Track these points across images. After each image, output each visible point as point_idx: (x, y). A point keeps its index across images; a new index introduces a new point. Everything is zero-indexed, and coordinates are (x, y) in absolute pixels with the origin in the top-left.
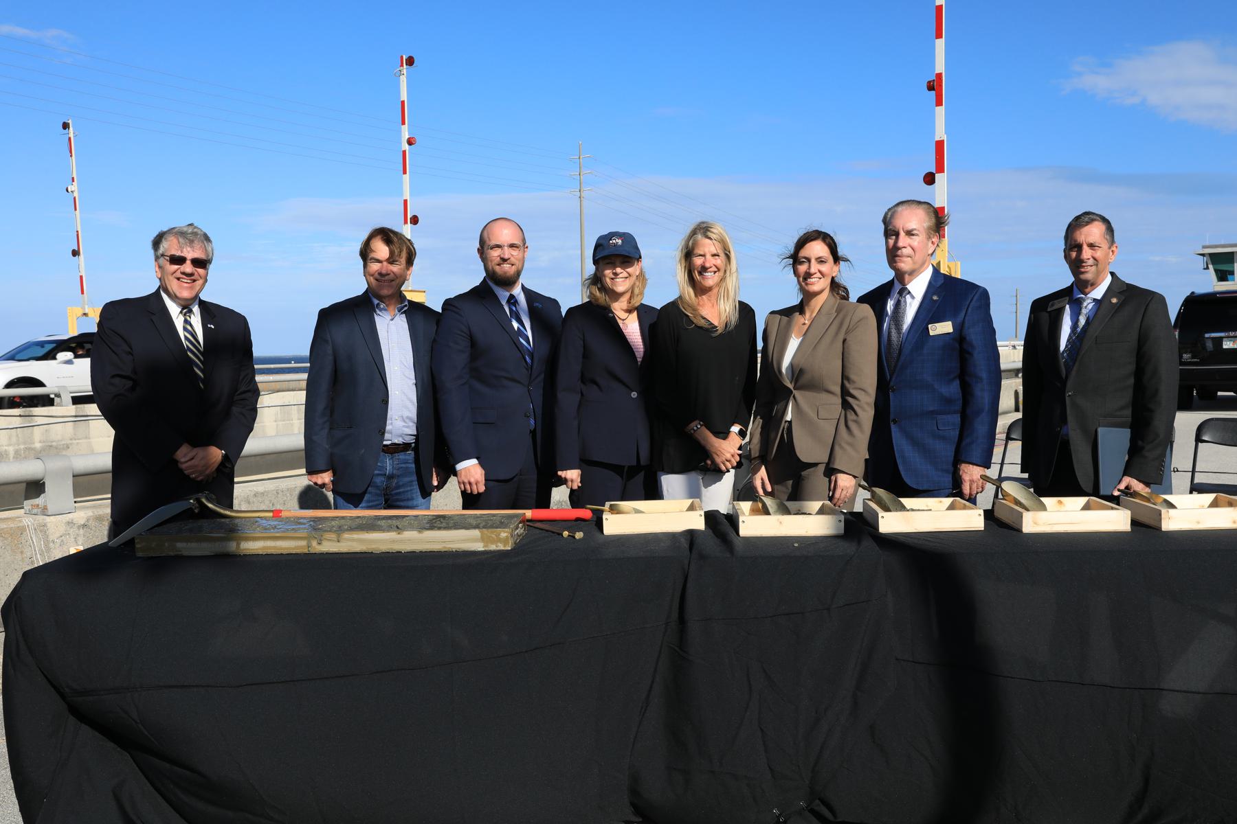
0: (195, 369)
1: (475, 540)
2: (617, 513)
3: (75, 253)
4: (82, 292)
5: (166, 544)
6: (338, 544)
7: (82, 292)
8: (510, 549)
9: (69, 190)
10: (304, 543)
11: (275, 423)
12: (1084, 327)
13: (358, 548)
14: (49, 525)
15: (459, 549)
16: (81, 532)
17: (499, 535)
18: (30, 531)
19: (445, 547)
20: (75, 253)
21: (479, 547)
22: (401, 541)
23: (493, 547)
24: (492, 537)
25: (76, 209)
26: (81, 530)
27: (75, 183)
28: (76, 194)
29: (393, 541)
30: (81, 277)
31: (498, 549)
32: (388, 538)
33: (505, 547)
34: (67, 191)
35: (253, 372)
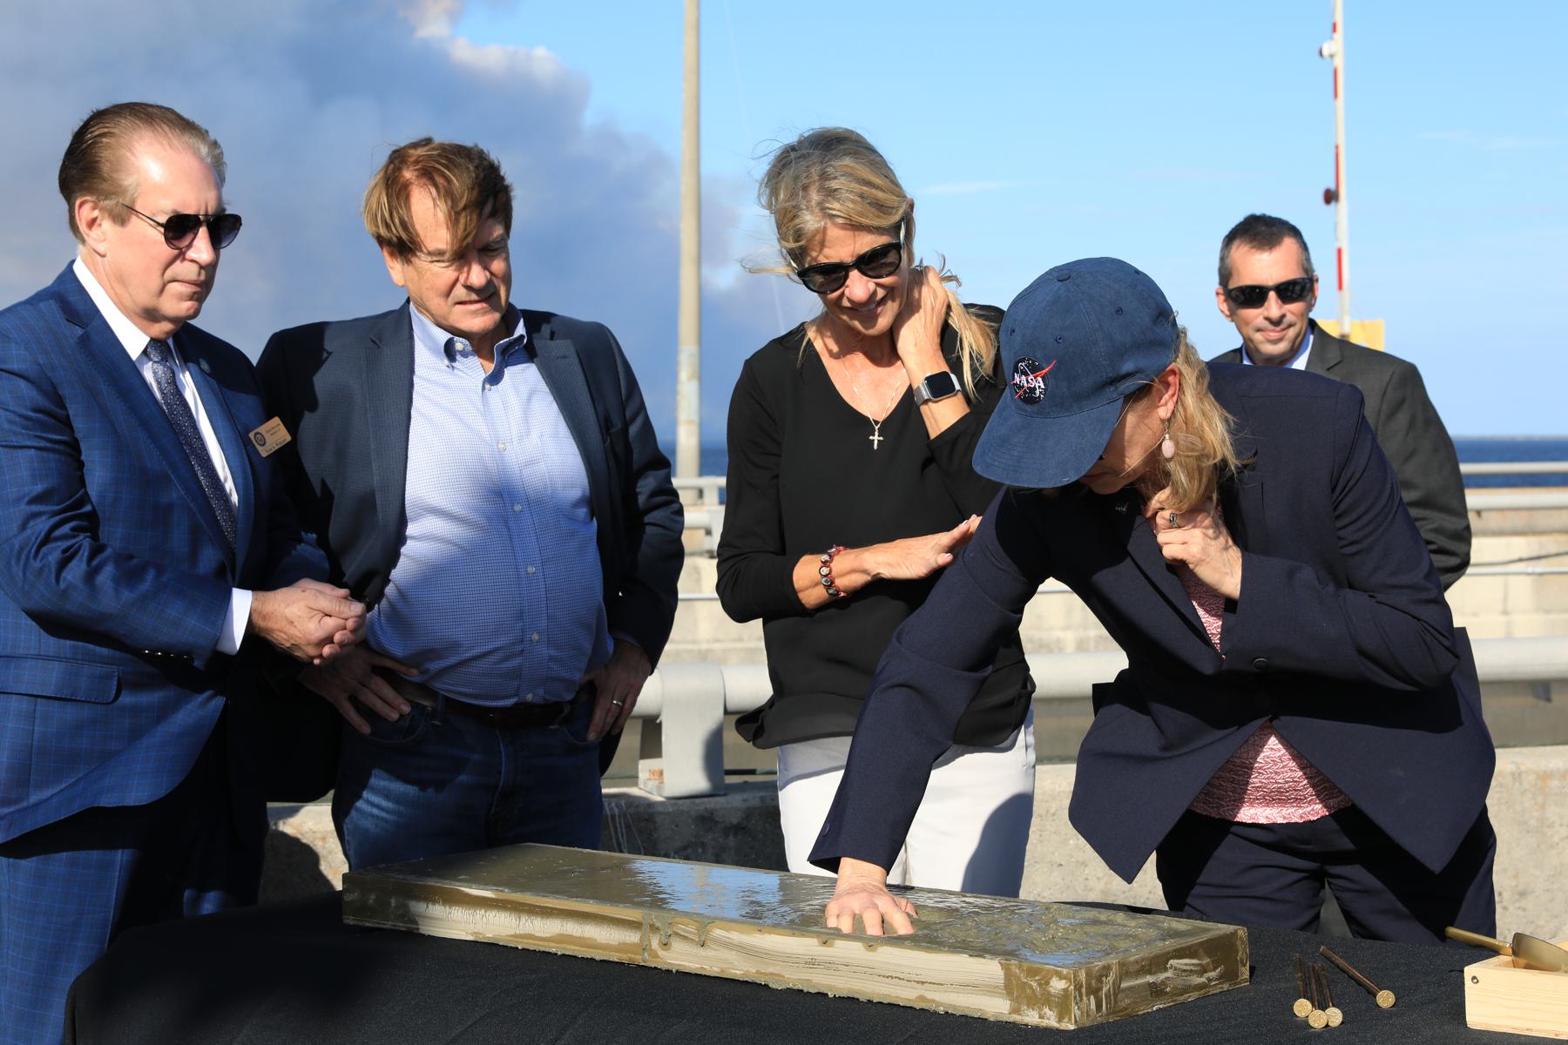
0: (235, 498)
1: (989, 990)
2: (1528, 967)
3: (1330, 197)
4: (1340, 287)
5: (393, 902)
6: (702, 952)
7: (1340, 287)
8: (1072, 1027)
9: (1326, 52)
10: (632, 937)
11: (1503, 619)
12: (79, 520)
13: (740, 968)
14: (658, 819)
15: (954, 1007)
16: (732, 841)
17: (1047, 983)
18: (616, 828)
19: (922, 998)
20: (1330, 197)
21: (996, 1007)
22: (829, 965)
23: (1031, 1017)
24: (1031, 987)
25: (1336, 95)
26: (731, 838)
27: (1339, 35)
28: (1339, 62)
29: (812, 963)
30: (1339, 252)
31: (1045, 1023)
32: (801, 951)
33: (1060, 1021)
34: (1321, 53)
35: (1459, 484)
